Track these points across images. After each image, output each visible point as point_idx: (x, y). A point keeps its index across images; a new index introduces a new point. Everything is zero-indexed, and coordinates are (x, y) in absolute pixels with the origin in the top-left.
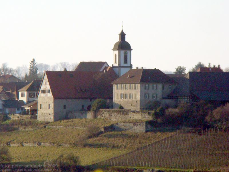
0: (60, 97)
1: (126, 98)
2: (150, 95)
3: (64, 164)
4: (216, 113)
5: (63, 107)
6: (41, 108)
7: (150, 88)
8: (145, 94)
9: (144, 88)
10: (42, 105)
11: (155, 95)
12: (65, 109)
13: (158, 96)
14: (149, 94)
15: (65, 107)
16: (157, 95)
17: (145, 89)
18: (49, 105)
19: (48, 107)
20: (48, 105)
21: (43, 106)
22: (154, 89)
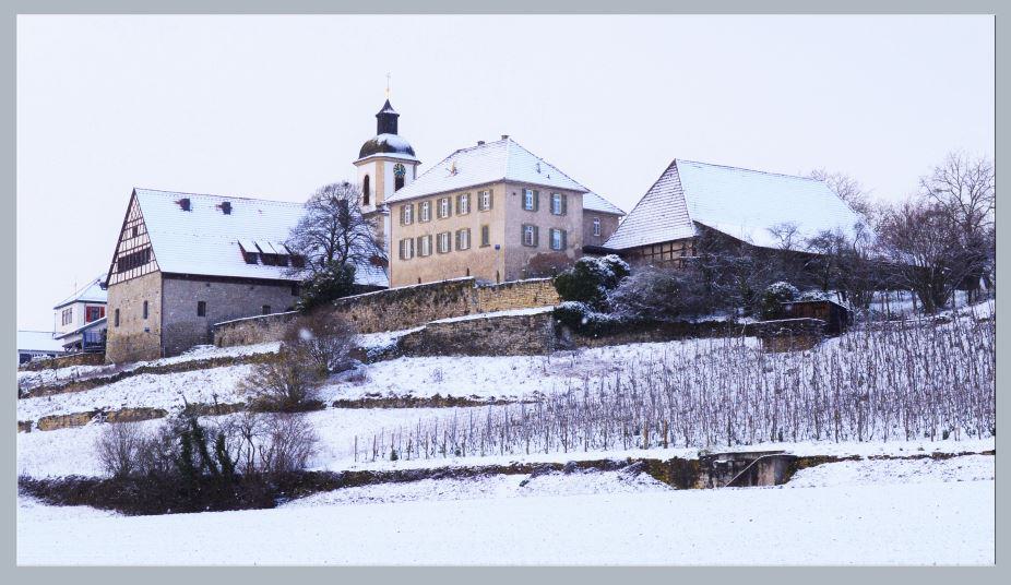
0: (198, 373)
1: (439, 251)
2: (540, 232)
3: (911, 416)
4: (518, 418)
5: (196, 309)
6: (117, 325)
7: (541, 204)
8: (524, 227)
9: (520, 203)
10: (121, 311)
11: (557, 236)
12: (202, 318)
13: (571, 239)
14: (536, 229)
15: (201, 309)
16: (564, 233)
17: (524, 206)
18: (146, 303)
19: (142, 314)
20: (142, 305)
21: (123, 316)
22: (556, 212)
